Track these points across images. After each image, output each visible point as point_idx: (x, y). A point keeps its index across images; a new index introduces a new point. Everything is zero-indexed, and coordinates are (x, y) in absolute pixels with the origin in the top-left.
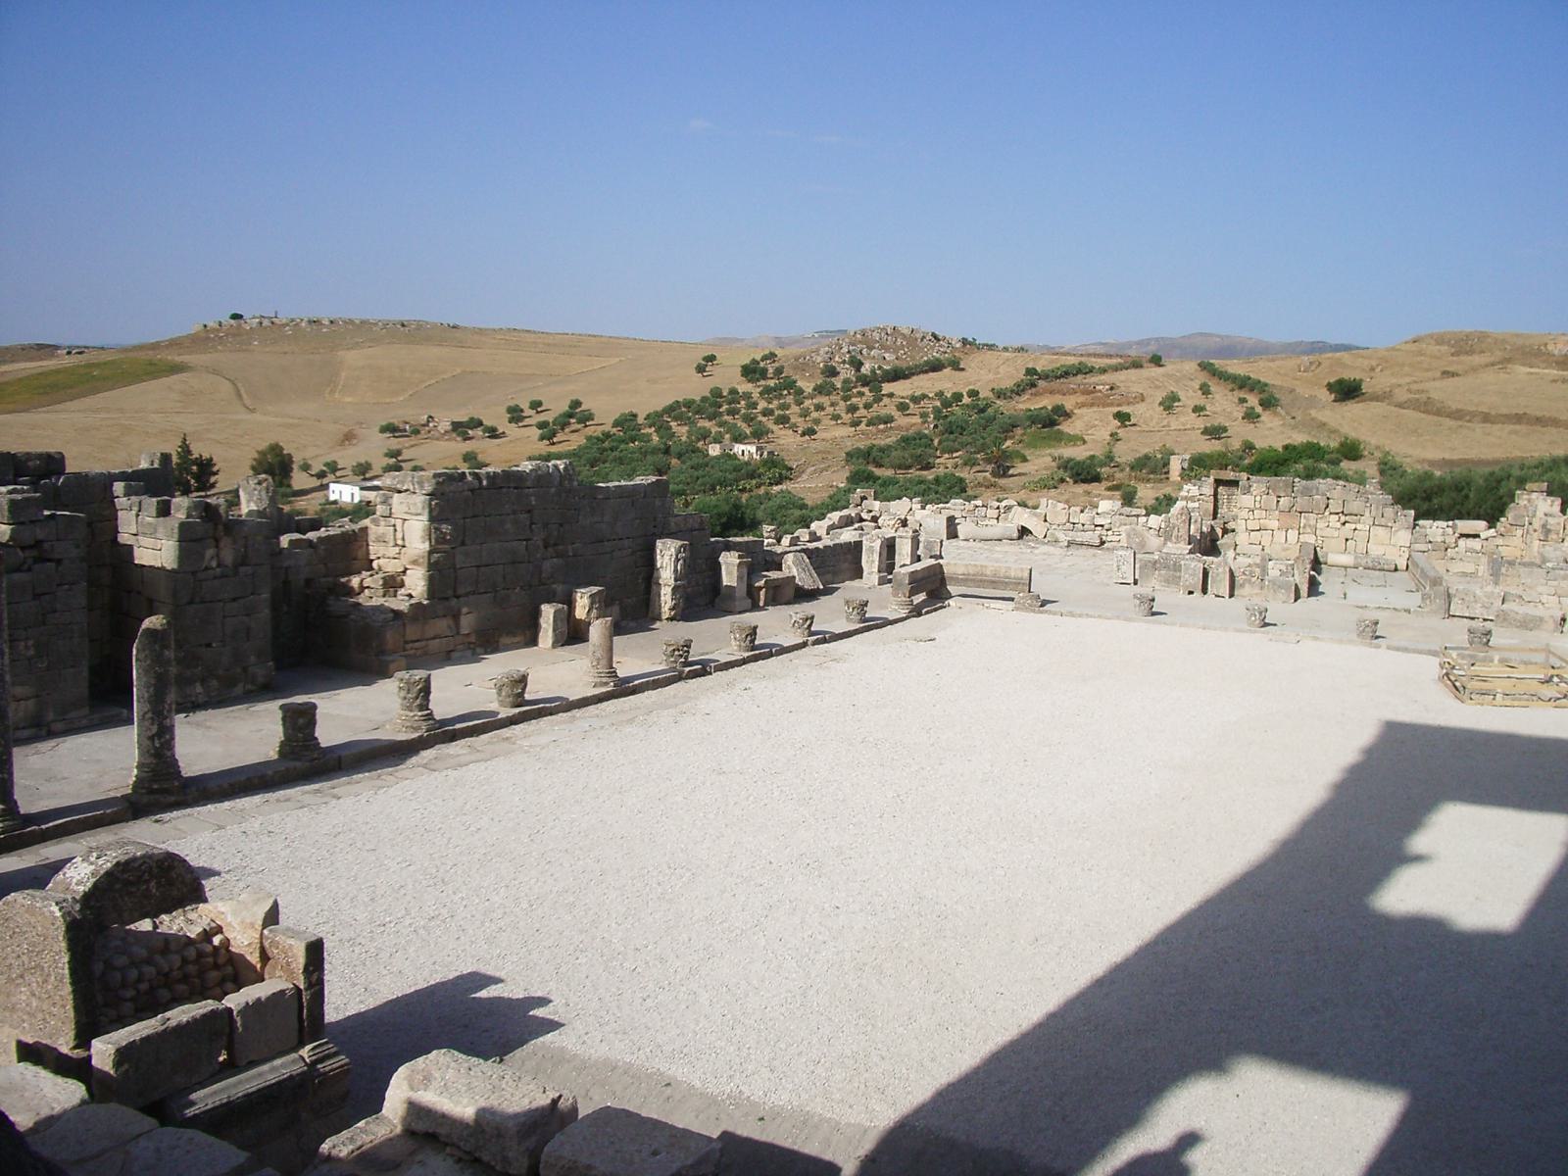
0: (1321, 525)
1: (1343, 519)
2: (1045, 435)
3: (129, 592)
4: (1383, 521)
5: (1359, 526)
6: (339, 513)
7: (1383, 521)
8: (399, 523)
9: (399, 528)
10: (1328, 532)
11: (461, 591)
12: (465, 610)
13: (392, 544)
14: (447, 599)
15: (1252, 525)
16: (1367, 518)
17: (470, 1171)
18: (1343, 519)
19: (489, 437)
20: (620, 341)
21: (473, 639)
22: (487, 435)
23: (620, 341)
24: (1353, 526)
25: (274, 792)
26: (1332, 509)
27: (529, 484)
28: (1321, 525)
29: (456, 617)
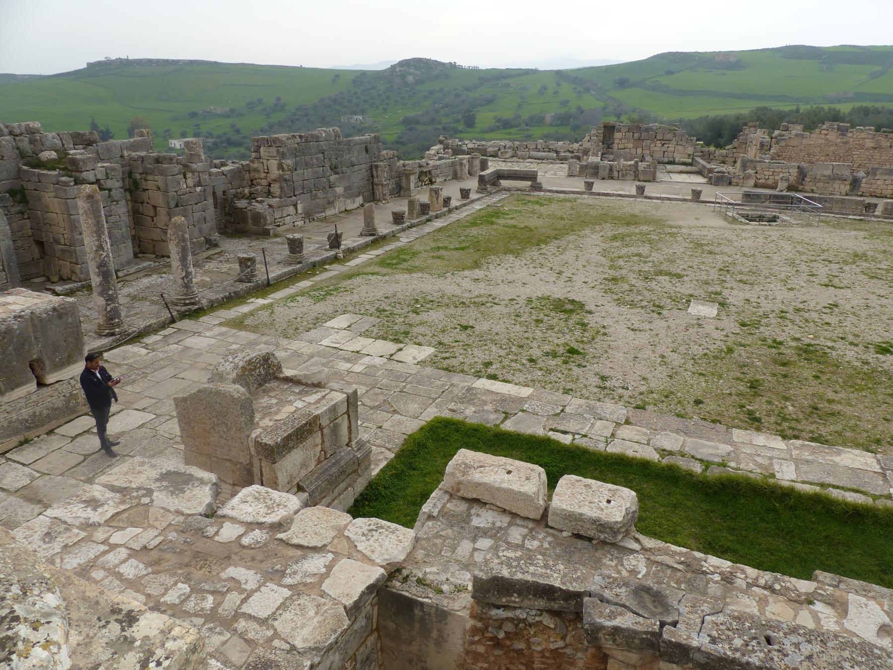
0: (652, 145)
1: (663, 142)
2: (233, 150)
3: (142, 203)
4: (681, 143)
5: (670, 145)
6: (131, 192)
7: (681, 143)
8: (265, 161)
9: (265, 165)
10: (655, 149)
11: (296, 193)
12: (299, 202)
13: (262, 171)
14: (291, 197)
15: (621, 146)
16: (674, 142)
17: (385, 574)
18: (663, 142)
19: (153, 573)
20: (63, 421)
21: (303, 216)
22: (150, 570)
23: (63, 421)
24: (667, 145)
25: (229, 309)
26: (658, 138)
27: (321, 139)
28: (652, 145)
29: (295, 206)
